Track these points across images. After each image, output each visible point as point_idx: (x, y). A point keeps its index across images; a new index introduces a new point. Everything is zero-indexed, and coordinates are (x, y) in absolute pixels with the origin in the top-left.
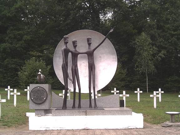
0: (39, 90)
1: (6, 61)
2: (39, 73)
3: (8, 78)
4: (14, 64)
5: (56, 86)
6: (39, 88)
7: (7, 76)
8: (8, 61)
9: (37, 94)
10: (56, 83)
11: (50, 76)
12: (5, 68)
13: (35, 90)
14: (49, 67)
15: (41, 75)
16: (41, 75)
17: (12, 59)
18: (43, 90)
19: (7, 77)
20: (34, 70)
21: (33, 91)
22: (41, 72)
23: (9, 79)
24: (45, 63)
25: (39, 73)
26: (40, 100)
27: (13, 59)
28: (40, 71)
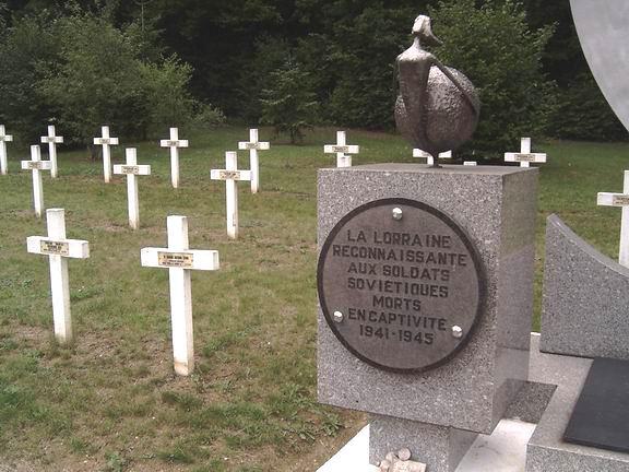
0: (397, 236)
1: (362, 16)
2: (413, 53)
3: (374, 88)
4: (393, 29)
5: (574, 124)
6: (397, 211)
7: (370, 82)
8: (369, 19)
9: (387, 271)
10: (577, 111)
11: (547, 79)
12: (363, 50)
13: (361, 237)
14: (545, 34)
15: (434, 72)
16: (434, 72)
17: (385, 6)
18: (439, 241)
19: (368, 86)
20: (466, 50)
21: (339, 240)
22: (426, 43)
23: (377, 92)
24: (523, 14)
25: (413, 53)
26: (407, 336)
27: (391, 11)
28: (420, 34)
